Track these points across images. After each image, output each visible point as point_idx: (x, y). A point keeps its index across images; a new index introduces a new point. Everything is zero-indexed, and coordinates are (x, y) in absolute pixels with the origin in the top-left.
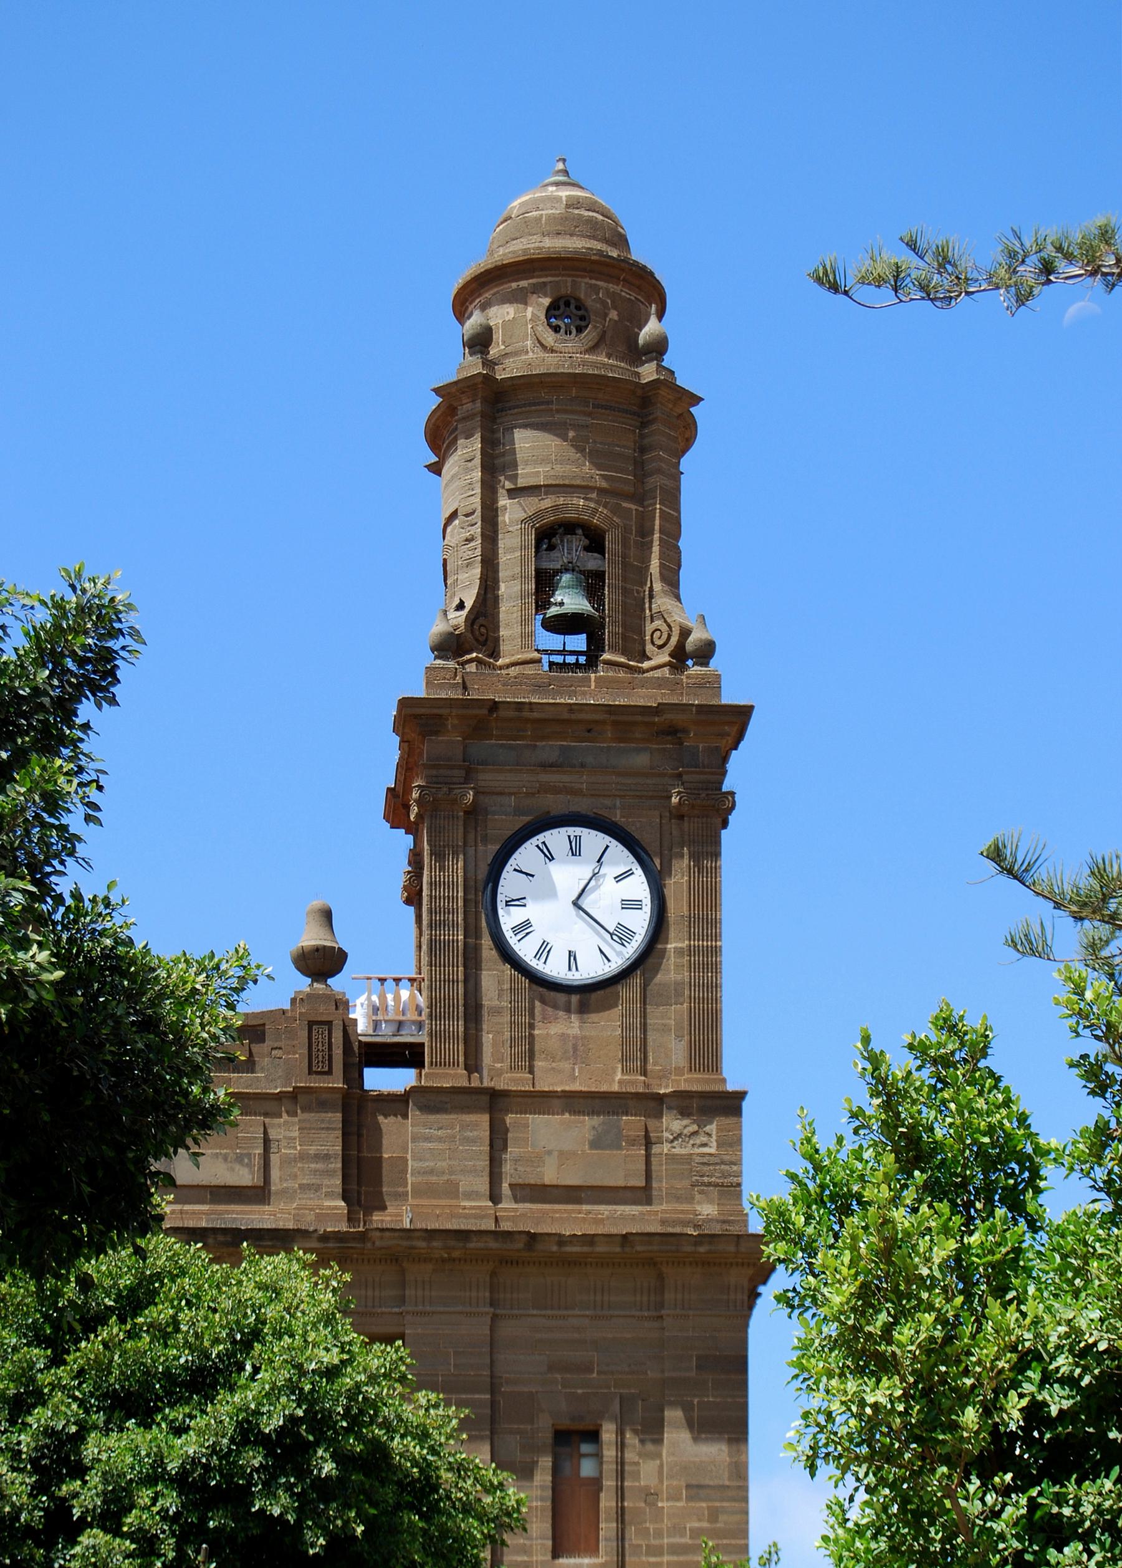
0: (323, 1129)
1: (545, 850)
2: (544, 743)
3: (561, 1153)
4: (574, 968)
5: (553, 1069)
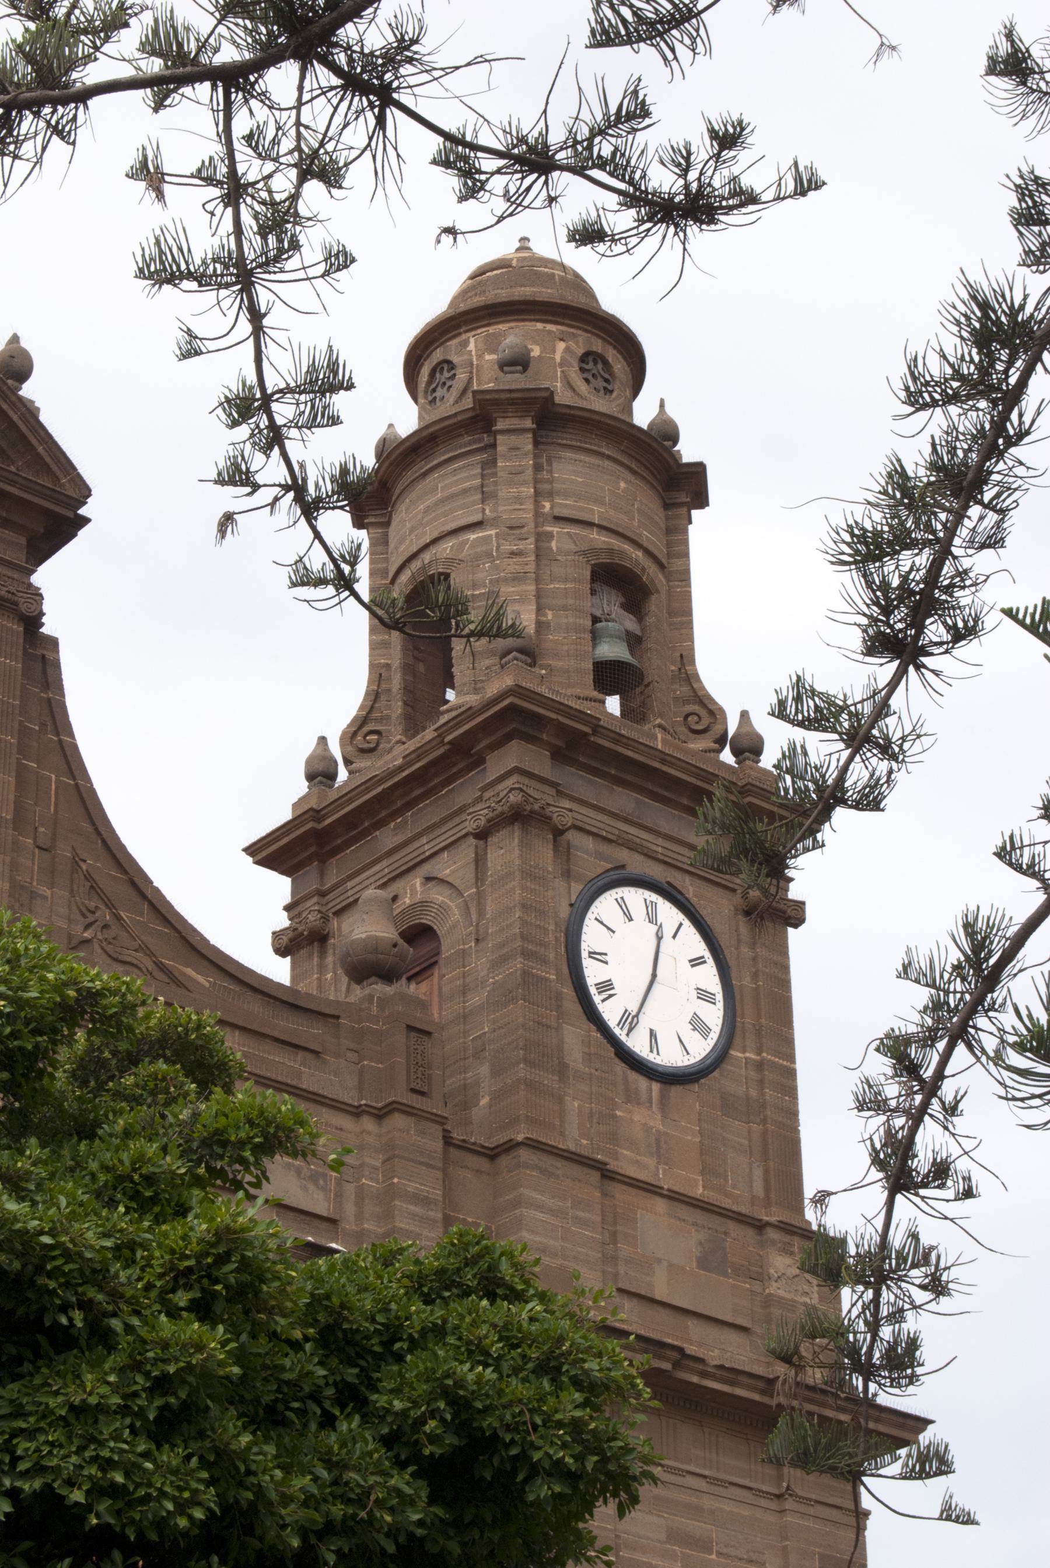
0: (422, 1163)
3: (670, 1266)
4: (655, 1050)
5: (638, 1162)
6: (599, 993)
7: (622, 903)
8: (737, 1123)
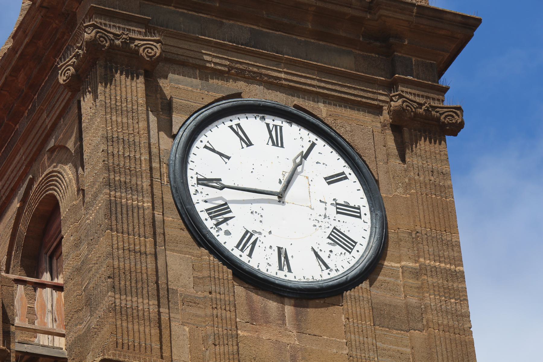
1: (240, 133)
2: (231, 22)
4: (286, 268)
6: (242, 250)
7: (238, 131)
8: (395, 332)
